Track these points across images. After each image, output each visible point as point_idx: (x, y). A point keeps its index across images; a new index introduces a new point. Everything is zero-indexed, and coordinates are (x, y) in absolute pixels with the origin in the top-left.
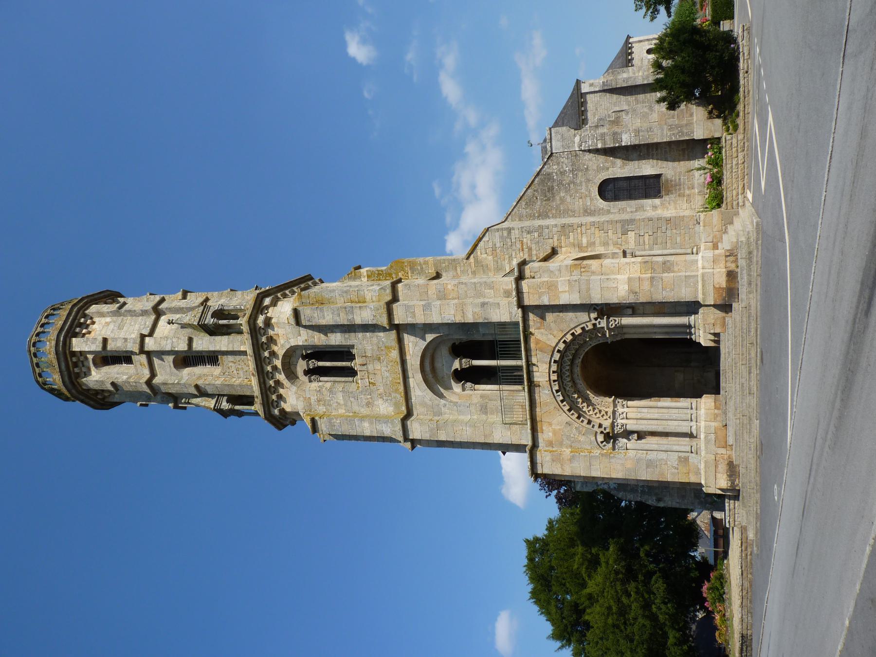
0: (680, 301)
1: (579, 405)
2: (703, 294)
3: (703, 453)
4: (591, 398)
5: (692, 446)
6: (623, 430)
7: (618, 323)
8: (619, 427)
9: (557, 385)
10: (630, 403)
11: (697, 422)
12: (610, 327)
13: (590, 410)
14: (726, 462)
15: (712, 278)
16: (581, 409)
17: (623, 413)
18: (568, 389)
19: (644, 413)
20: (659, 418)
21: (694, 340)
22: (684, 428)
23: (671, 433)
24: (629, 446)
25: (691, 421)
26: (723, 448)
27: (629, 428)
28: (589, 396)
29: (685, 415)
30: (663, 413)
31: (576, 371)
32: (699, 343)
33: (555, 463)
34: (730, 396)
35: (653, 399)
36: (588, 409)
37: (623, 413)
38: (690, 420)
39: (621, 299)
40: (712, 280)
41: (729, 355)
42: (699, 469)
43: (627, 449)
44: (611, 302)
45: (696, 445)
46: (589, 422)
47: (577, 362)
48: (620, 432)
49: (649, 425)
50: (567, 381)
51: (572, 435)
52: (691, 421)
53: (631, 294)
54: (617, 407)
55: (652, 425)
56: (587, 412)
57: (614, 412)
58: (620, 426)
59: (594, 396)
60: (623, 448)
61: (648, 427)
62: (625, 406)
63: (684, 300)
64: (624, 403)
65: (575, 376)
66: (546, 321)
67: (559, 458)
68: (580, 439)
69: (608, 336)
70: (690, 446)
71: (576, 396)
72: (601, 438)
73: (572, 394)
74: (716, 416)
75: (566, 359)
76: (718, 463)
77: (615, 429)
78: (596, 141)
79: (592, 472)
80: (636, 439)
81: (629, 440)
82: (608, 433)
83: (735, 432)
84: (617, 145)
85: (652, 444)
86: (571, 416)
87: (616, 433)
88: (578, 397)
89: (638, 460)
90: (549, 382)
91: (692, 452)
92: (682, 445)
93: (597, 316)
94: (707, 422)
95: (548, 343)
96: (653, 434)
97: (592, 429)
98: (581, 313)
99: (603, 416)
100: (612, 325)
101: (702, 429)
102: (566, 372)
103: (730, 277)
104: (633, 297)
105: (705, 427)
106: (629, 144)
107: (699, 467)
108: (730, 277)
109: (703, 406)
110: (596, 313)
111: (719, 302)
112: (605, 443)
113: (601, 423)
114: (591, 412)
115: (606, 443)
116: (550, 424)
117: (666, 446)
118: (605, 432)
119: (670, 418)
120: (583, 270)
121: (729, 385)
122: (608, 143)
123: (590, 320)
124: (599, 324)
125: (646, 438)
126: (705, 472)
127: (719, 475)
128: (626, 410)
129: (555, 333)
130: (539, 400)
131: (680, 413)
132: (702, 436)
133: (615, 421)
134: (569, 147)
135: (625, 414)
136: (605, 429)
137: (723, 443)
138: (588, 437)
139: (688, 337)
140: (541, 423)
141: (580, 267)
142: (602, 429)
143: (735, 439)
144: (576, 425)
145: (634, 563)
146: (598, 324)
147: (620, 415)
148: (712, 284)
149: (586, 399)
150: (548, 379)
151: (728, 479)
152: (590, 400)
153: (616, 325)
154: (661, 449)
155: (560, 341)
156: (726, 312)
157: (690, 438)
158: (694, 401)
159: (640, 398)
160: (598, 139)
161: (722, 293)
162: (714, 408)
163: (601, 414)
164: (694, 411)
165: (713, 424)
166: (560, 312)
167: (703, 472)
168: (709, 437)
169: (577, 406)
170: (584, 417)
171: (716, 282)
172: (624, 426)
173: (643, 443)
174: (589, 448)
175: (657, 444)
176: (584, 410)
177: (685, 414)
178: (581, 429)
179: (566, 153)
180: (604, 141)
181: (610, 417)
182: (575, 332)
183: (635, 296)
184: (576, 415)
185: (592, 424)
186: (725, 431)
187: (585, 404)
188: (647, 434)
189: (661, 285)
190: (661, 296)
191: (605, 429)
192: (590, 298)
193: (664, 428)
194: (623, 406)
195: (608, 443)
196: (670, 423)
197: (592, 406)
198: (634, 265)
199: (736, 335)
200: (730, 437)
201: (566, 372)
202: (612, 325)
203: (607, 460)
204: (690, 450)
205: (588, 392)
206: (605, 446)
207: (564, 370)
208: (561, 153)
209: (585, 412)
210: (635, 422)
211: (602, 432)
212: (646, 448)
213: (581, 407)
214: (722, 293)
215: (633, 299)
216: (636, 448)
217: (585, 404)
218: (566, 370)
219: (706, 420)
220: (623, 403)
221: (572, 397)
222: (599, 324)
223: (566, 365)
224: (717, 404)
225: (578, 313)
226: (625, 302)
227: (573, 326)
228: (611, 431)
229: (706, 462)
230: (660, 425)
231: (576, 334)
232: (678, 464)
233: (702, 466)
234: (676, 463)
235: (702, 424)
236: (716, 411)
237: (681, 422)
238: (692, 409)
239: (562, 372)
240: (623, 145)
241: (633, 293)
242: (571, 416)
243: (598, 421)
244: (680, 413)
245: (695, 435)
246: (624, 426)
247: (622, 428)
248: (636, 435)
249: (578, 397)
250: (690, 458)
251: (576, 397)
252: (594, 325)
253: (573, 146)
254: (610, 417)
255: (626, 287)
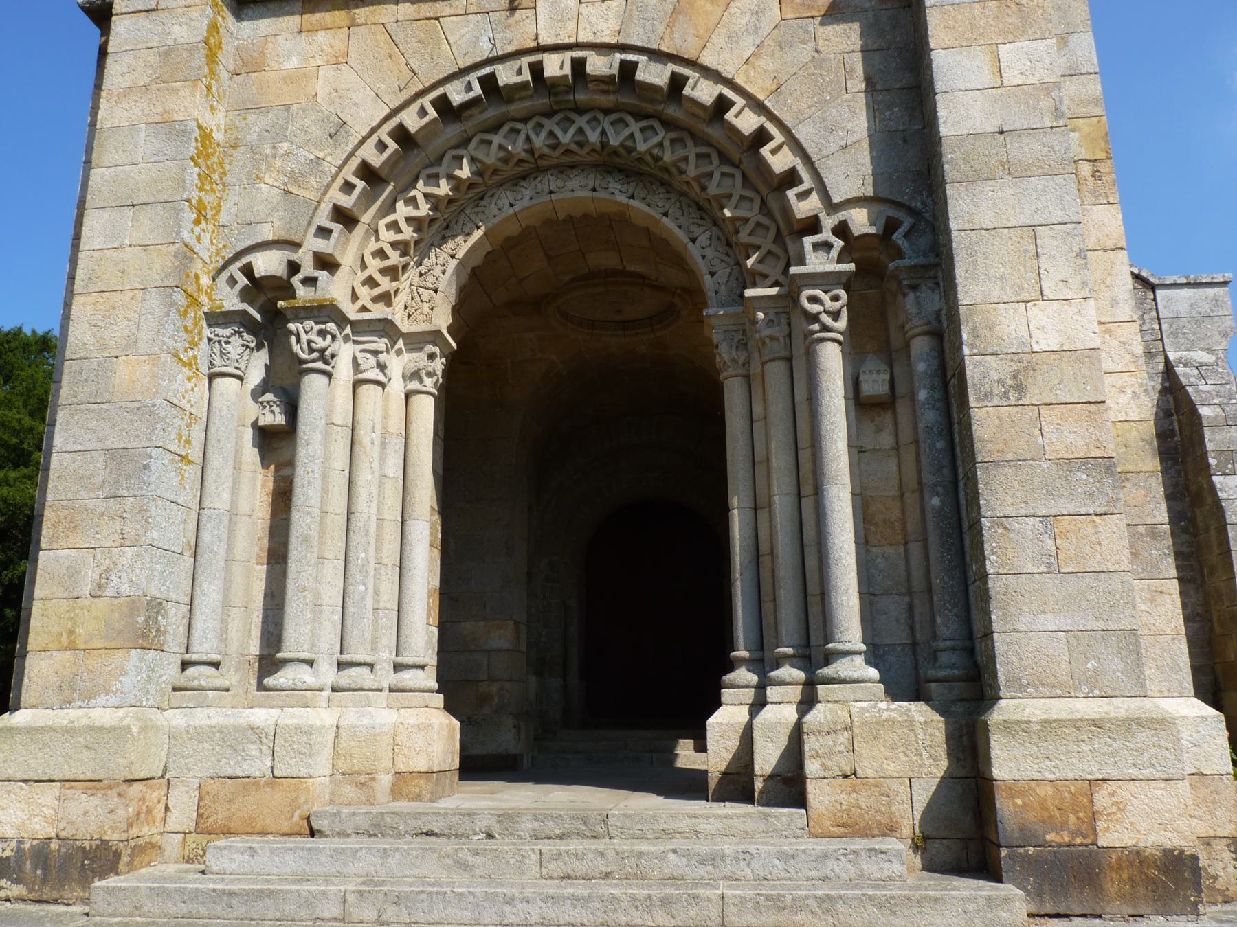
0: (994, 605)
1: (420, 184)
2: (1050, 726)
3: (177, 719)
4: (451, 244)
5: (216, 665)
6: (304, 356)
7: (826, 328)
8: (319, 340)
9: (517, 79)
10: (425, 409)
11: (334, 690)
12: (806, 293)
13: (399, 231)
14: (113, 836)
15: (1147, 773)
16: (402, 191)
17: (382, 367)
18: (497, 139)
19: (382, 459)
20: (359, 521)
21: (730, 677)
22: (307, 629)
23: (284, 574)
24: (226, 386)
25: (341, 665)
26: (199, 816)
27: (313, 386)
28: (460, 239)
29: (368, 636)
30: (379, 540)
31: (571, 184)
32: (716, 704)
33: (152, 58)
34: (470, 859)
35: (437, 518)
36: (403, 225)
37: (382, 367)
38: (346, 657)
39: (979, 319)
40: (1134, 772)
41: (703, 861)
42: (89, 697)
43: (211, 377)
44: (959, 272)
45: (219, 683)
46: (346, 218)
47: (614, 186)
48: (296, 347)
49: (325, 477)
50: (533, 136)
51: (285, 146)
52: (341, 665)
53: (1008, 367)
54: (410, 350)
55: (325, 490)
56: (390, 218)
57: (386, 328)
58: (320, 343)
59: (460, 255)
60: (217, 361)
61: (317, 467)
62: (414, 385)
63: (996, 626)
64: (428, 382)
65: (551, 181)
66: (822, 24)
67: (181, 75)
68: (267, 178)
69: (749, 293)
70: (215, 657)
71: (465, 172)
72: (268, 264)
73: (473, 160)
74: (363, 781)
75: (635, 127)
76: (112, 793)
77: (309, 323)
78: (1216, 401)
79: (105, 214)
80: (261, 423)
81: (256, 394)
82: (289, 292)
83: (271, 893)
84: (1212, 461)
85: (235, 490)
86: (374, 139)
87: (292, 326)
88: (457, 183)
89: (151, 414)
90: (533, 44)
91: (185, 665)
92: (224, 622)
93: (856, 233)
94: (331, 737)
95: (719, 39)
96: (283, 498)
97: (313, 229)
98: (868, 170)
99: (371, 282)
100: (814, 300)
101: (294, 716)
102: (572, 131)
103: (1164, 869)
104: (994, 376)
105: (306, 731)
106: (1222, 495)
107: (101, 700)
108: (1164, 869)
109: (411, 717)
110: (872, 230)
111: (1006, 807)
112: (243, 281)
113: (339, 273)
114: (387, 236)
115: (245, 288)
116: (338, 60)
117: (220, 548)
118: (296, 281)
119: (354, 570)
120: (1086, 169)
121: (535, 857)
122: (1217, 437)
123: (832, 207)
124: (816, 246)
125: (265, 463)
126: (69, 731)
127: (48, 796)
128: (397, 387)
129: (767, 63)
130: (448, 11)
131: (376, 620)
132: (262, 716)
133: (348, 330)
134: (1175, 334)
135: (375, 374)
136: (310, 281)
137: (219, 817)
138: (274, 210)
139: (741, 653)
140: (346, 23)
141: (1100, 155)
142: (308, 269)
143: (232, 894)
144: (333, 160)
145: (12, 549)
146: (817, 238)
147: (375, 353)
148: (1114, 774)
149: (447, 228)
150: (546, 39)
151: (27, 846)
152: (444, 239)
153: (815, 318)
154: (207, 526)
155: (730, 83)
156: (926, 838)
157: (261, 658)
158: (428, 679)
159: (441, 472)
160: (1228, 409)
161: (1064, 825)
162: (402, 768)
163: (378, 277)
164: (387, 678)
165: (321, 767)
166: (868, 80)
167: (72, 715)
168: (253, 749)
169: (416, 180)
170: (367, 199)
171: (1125, 792)
172: (320, 365)
173: (238, 453)
174: (223, 218)
175: (233, 513)
176: (400, 205)
177: (375, 640)
178: (312, 181)
179: (1157, 327)
180: (1223, 422)
181: (364, 309)
182: (772, 145)
183: (1001, 382)
184: (377, 160)
185: (337, 228)
186: (286, 826)
187: (424, 209)
188: (285, 472)
189: (1071, 508)
190: (1009, 511)
191: (310, 281)
192: (979, 177)
193: (306, 539)
194: (416, 375)
195: (245, 295)
196: (332, 572)
197: (417, 243)
198: (1129, 391)
199: (840, 907)
200: (246, 857)
201: (572, 131)
202: (814, 300)
203: (156, 276)
204: (195, 657)
205: (478, 234)
206: (232, 281)
207: (581, 121)
208: (1154, 314)
209: (390, 207)
210: (342, 414)
211: (294, 268)
212: (215, 461)
213: (413, 193)
214: (1057, 829)
215: (985, 375)
216: (215, 419)
217: (424, 209)
218: (580, 131)
219: (343, 734)
220: (429, 374)
221: (460, 158)
222: (816, 246)
223: (608, 128)
224: (422, 782)
225: (867, 152)
226: (965, 336)
227: (803, 133)
228: (298, 303)
229: (119, 733)
230: (322, 524)
231: (765, 151)
232: (118, 596)
233: (102, 714)
234: (125, 590)
235: (322, 716)
236: (386, 780)
237: (337, 617)
238: (398, 667)
239: (573, 116)
240: (1214, 478)
241: (1015, 376)
242: (374, 139)
243: (347, 259)
244: (376, 620)
245: (269, 681)
246: (320, 365)
247: (311, 351)
248: (280, 419)
249: (457, 183)
250: (152, 654)
251: (457, 173)
252: (813, 225)
253: (1178, 347)
254: (364, 309)
255: (1046, 341)
